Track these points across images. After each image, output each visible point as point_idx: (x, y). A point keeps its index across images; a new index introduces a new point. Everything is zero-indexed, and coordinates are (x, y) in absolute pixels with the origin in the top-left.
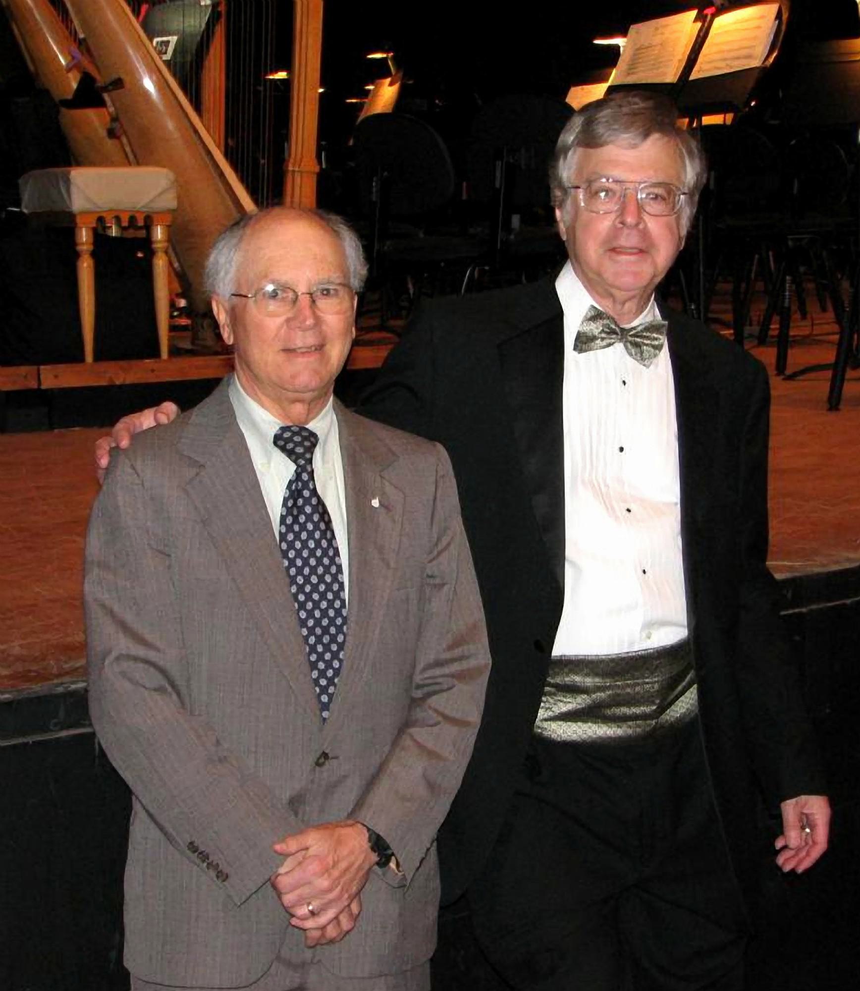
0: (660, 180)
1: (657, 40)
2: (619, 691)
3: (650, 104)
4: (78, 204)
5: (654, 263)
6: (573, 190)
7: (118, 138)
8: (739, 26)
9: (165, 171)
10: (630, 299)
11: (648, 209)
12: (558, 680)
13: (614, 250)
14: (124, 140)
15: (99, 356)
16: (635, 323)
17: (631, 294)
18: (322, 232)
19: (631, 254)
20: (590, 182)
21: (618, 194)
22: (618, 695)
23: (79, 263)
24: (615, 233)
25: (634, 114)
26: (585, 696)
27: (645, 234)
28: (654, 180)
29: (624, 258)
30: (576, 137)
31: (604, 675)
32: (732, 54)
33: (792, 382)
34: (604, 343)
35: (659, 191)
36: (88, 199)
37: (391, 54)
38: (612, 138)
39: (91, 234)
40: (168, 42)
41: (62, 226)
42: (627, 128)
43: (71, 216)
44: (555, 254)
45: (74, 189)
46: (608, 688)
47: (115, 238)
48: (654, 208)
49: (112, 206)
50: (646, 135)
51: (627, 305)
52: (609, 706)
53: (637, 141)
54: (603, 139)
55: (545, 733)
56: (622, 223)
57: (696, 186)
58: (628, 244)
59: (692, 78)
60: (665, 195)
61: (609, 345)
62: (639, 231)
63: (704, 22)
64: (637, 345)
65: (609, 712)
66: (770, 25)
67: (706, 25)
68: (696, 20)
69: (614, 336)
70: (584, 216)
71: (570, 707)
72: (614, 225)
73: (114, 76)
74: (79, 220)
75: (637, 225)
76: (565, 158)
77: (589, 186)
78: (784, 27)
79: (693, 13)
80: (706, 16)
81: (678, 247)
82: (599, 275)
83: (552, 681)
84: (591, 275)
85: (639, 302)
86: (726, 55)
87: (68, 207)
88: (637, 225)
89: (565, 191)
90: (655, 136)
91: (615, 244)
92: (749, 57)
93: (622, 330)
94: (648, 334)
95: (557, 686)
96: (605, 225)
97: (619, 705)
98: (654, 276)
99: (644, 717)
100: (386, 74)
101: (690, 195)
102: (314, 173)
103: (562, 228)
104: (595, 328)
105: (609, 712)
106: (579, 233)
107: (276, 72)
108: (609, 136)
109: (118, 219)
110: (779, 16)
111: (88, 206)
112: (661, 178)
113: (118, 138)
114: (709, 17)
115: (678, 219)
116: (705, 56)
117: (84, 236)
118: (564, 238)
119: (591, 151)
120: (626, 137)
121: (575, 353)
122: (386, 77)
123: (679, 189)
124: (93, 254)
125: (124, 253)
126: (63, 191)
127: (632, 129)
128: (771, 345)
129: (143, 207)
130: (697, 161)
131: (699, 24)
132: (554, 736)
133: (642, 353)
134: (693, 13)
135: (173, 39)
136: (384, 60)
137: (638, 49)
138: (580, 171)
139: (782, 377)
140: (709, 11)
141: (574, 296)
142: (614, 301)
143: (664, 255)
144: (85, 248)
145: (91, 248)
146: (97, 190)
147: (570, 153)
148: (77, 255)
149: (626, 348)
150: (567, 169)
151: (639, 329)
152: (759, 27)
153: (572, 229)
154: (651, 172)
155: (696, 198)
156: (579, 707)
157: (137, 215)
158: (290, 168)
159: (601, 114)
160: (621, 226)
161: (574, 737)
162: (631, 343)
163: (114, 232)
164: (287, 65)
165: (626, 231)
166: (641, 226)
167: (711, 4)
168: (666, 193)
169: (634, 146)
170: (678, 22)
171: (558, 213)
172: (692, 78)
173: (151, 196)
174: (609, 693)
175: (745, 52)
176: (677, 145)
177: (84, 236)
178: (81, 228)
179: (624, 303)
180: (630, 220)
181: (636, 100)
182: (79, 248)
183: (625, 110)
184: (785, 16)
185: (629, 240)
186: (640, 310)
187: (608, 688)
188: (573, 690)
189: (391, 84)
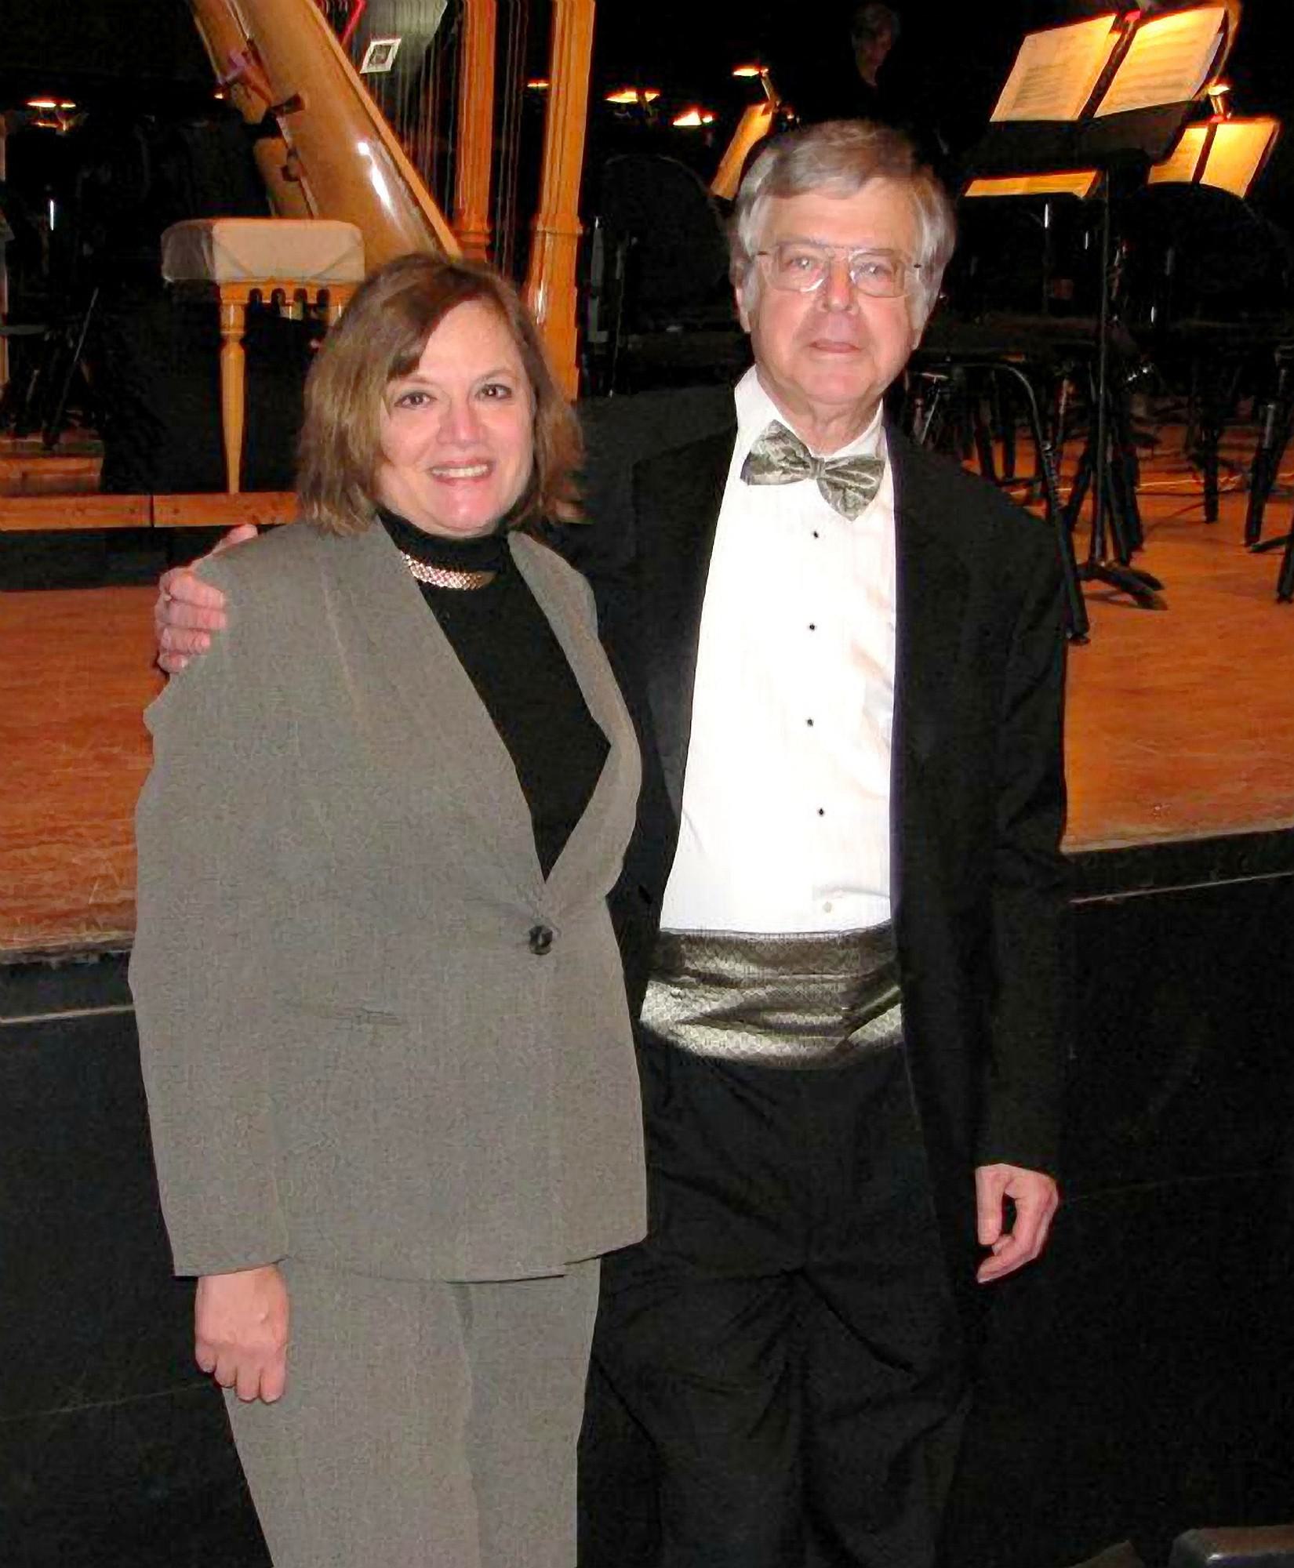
0: (885, 245)
1: (1058, 59)
2: (784, 989)
3: (874, 135)
4: (223, 270)
5: (874, 365)
6: (758, 258)
7: (297, 179)
8: (1168, 39)
9: (349, 226)
10: (838, 416)
11: (862, 286)
12: (697, 966)
13: (814, 345)
14: (305, 183)
15: (246, 486)
16: (837, 455)
17: (839, 408)
18: (485, 315)
19: (840, 351)
20: (781, 248)
21: (822, 265)
22: (784, 994)
23: (224, 352)
24: (816, 320)
25: (849, 150)
26: (734, 991)
27: (859, 324)
28: (874, 245)
29: (829, 357)
30: (765, 181)
31: (761, 961)
32: (1158, 80)
33: (1260, 556)
34: (788, 477)
35: (881, 261)
36: (236, 264)
37: (765, 71)
38: (815, 182)
39: (241, 312)
40: (389, 47)
41: (204, 300)
42: (838, 170)
43: (213, 288)
44: (741, 353)
45: (216, 248)
46: (770, 982)
47: (294, 321)
48: (874, 284)
49: (271, 273)
50: (864, 177)
51: (834, 424)
52: (771, 1009)
53: (852, 187)
54: (802, 184)
55: (682, 1042)
56: (826, 306)
57: (936, 258)
58: (833, 338)
59: (1097, 115)
60: (891, 268)
61: (793, 481)
62: (850, 317)
63: (1124, 31)
64: (836, 486)
65: (773, 1018)
66: (1212, 37)
67: (1126, 37)
68: (1114, 28)
69: (800, 469)
70: (774, 295)
71: (716, 1006)
72: (814, 309)
73: (291, 94)
74: (223, 293)
75: (848, 308)
76: (749, 213)
77: (781, 251)
78: (1229, 44)
79: (1110, 20)
80: (1128, 24)
81: (910, 346)
82: (792, 380)
83: (692, 967)
84: (781, 382)
85: (851, 422)
86: (1151, 82)
87: (208, 273)
88: (848, 308)
89: (749, 261)
90: (876, 182)
91: (814, 339)
92: (1178, 85)
93: (815, 461)
94: (855, 473)
95: (696, 974)
96: (801, 311)
97: (786, 1008)
98: (872, 386)
99: (825, 1030)
100: (760, 98)
101: (930, 269)
102: (572, 235)
103: (744, 315)
104: (774, 452)
105: (773, 1018)
106: (766, 326)
107: (622, 91)
108: (812, 179)
109: (301, 295)
110: (1224, 27)
111: (238, 274)
112: (884, 242)
113: (297, 179)
114: (1130, 28)
115: (909, 302)
116: (1120, 82)
117: (233, 319)
118: (747, 329)
119: (784, 202)
120: (835, 181)
121: (743, 484)
122: (759, 102)
123: (909, 260)
124: (243, 342)
125: (287, 338)
126: (204, 246)
127: (845, 169)
128: (1280, 500)
129: (315, 277)
130: (940, 220)
131: (1117, 36)
132: (693, 1047)
133: (844, 500)
134: (1110, 20)
135: (396, 43)
136: (758, 78)
137: (1031, 70)
138: (769, 229)
139: (1251, 548)
140: (1132, 18)
141: (755, 408)
142: (815, 418)
143: (887, 357)
144: (232, 332)
145: (241, 332)
146: (244, 253)
147: (756, 206)
148: (221, 342)
149: (822, 490)
150: (750, 230)
151: (841, 464)
152: (1194, 42)
153: (755, 317)
154: (870, 235)
155: (939, 274)
156: (727, 1007)
157: (308, 289)
158: (540, 228)
159: (799, 149)
160: (824, 310)
161: (722, 1052)
162: (829, 483)
163: (291, 313)
164: (546, 76)
165: (831, 318)
166: (853, 312)
167: (1134, 7)
168: (891, 265)
169: (844, 196)
170: (1089, 32)
171: (738, 292)
172: (1097, 115)
173: (332, 258)
174: (770, 989)
175: (1171, 78)
176: (910, 197)
177: (233, 319)
178: (228, 305)
179: (828, 422)
180: (836, 301)
181: (854, 131)
182: (225, 332)
183: (838, 143)
184: (1233, 27)
185: (836, 331)
186: (853, 434)
187: (770, 982)
188: (719, 981)
189: (765, 112)
